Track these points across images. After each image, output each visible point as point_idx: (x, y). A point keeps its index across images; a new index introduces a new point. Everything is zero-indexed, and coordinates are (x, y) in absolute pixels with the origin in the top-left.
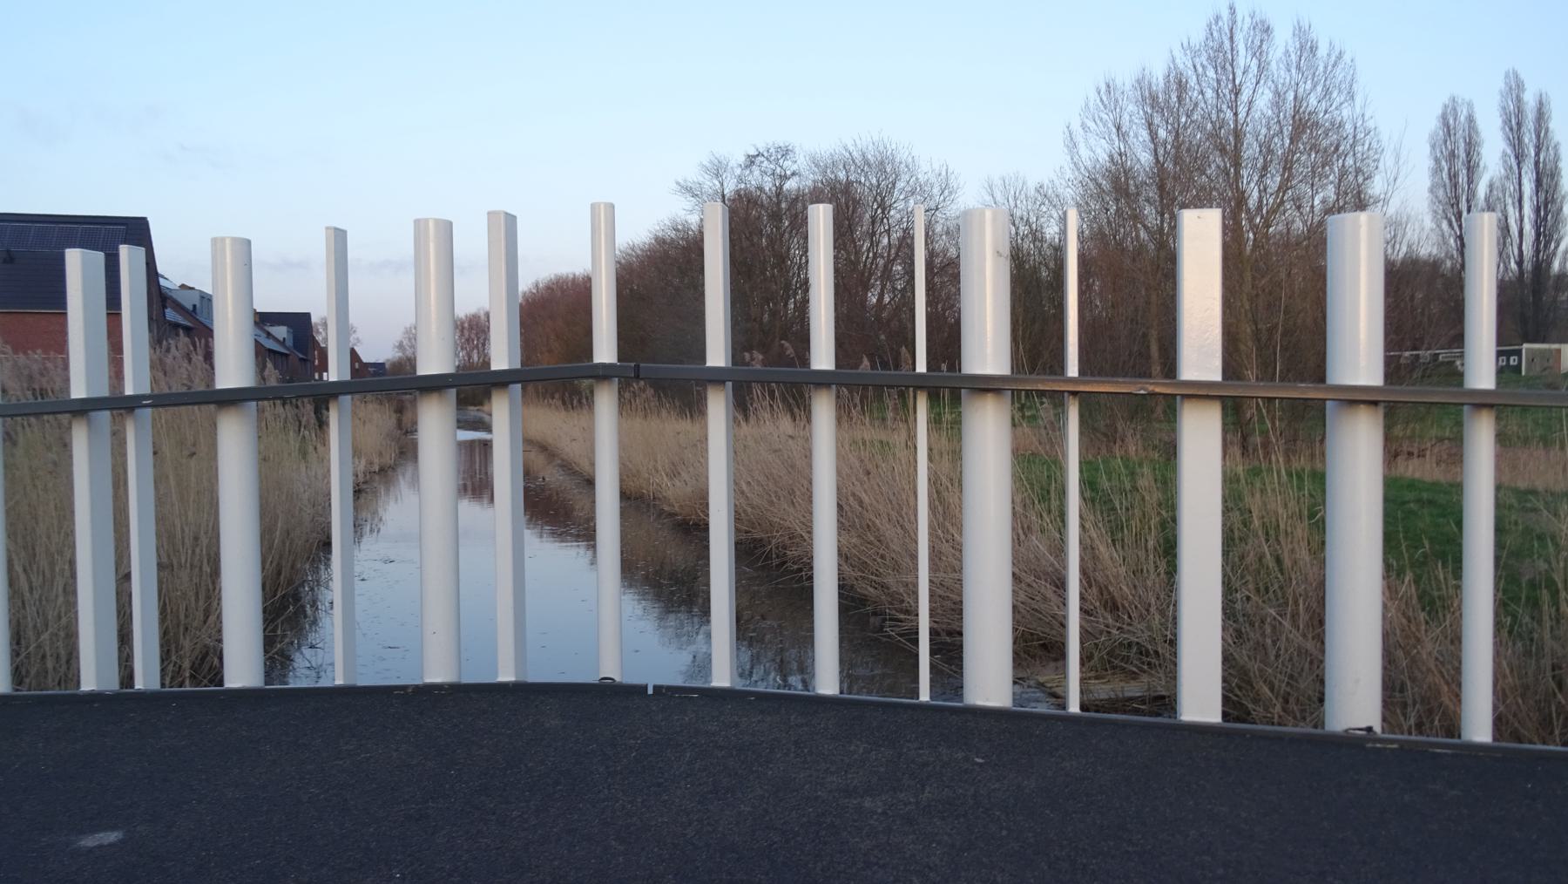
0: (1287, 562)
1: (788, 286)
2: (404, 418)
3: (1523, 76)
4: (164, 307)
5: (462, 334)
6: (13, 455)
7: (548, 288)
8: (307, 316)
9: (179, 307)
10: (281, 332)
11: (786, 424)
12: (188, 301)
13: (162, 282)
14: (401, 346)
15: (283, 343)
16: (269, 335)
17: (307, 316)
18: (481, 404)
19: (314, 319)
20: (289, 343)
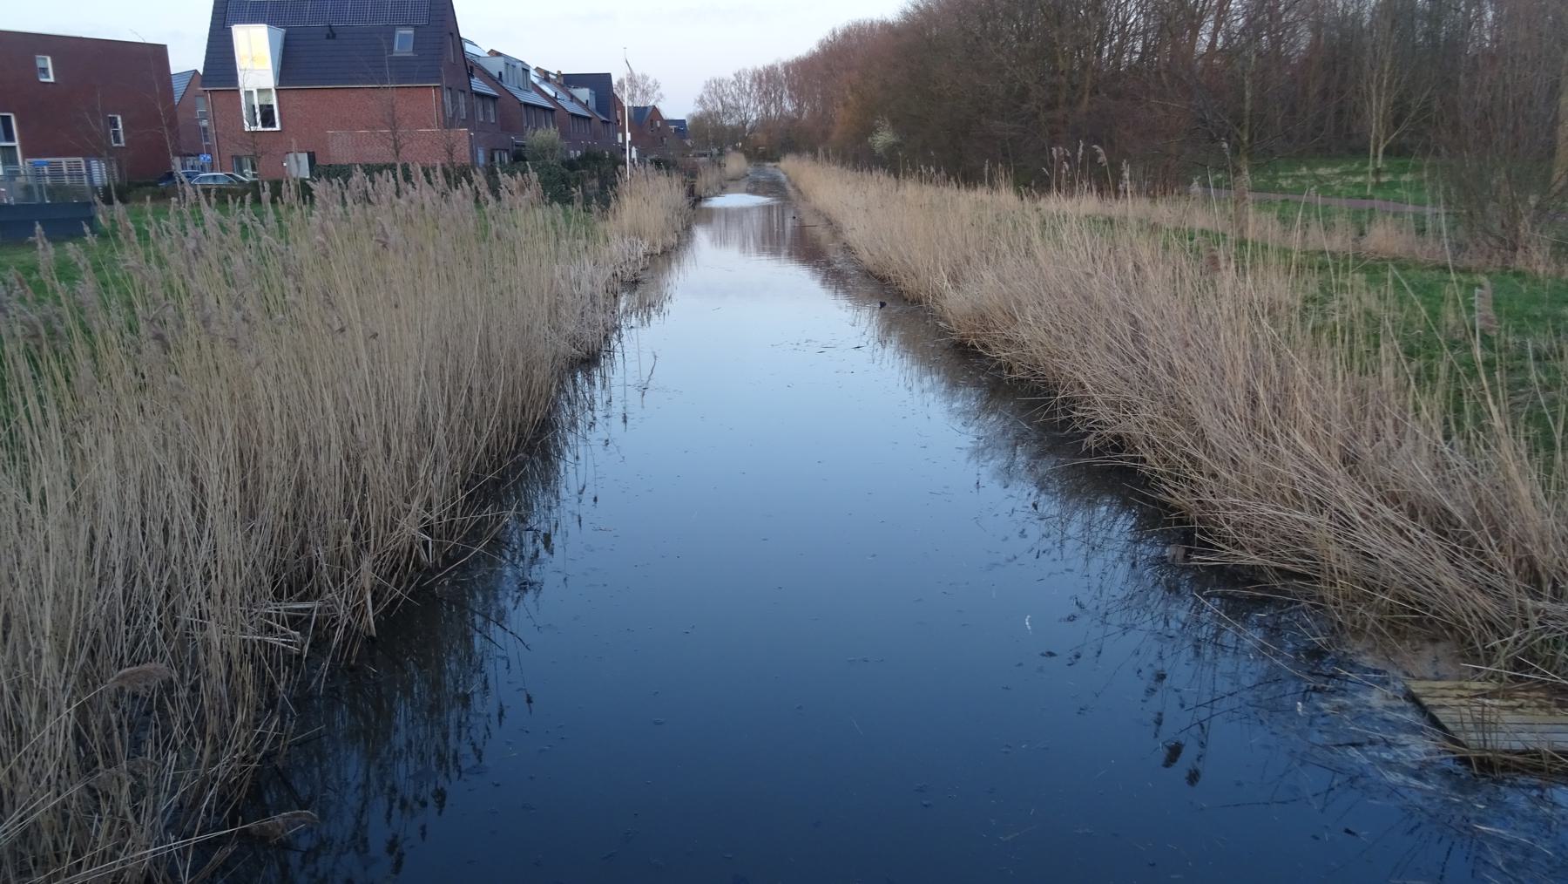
0: (1290, 535)
1: (1103, 29)
2: (698, 185)
3: (1184, 750)
4: (471, 75)
5: (760, 87)
6: (108, 201)
7: (847, 35)
8: (608, 77)
9: (486, 76)
10: (584, 94)
11: (1148, 207)
12: (495, 67)
13: (468, 48)
14: (701, 101)
15: (585, 106)
16: (572, 97)
17: (608, 77)
18: (778, 160)
19: (615, 82)
20: (592, 105)
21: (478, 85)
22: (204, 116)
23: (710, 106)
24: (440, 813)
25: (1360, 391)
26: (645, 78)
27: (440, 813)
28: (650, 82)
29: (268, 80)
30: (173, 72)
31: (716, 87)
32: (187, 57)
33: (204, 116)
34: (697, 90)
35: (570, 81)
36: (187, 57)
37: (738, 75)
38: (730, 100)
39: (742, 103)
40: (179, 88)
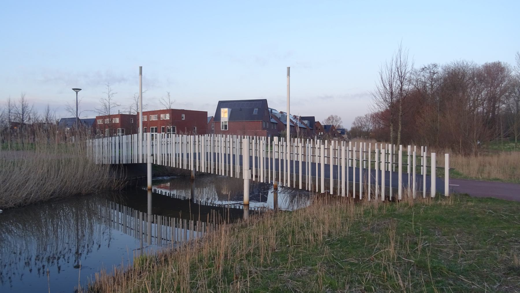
10: (306, 122)
14: (354, 123)
15: (306, 125)
17: (206, 113)
20: (308, 125)
21: (273, 120)
22: (213, 127)
23: (357, 125)
24: (98, 249)
25: (513, 173)
26: (336, 116)
27: (98, 249)
28: (338, 118)
29: (227, 120)
30: (208, 116)
31: (359, 119)
32: (211, 113)
33: (213, 127)
34: (353, 120)
35: (302, 119)
36: (211, 113)
37: (366, 116)
38: (363, 123)
39: (367, 124)
40: (209, 121)
